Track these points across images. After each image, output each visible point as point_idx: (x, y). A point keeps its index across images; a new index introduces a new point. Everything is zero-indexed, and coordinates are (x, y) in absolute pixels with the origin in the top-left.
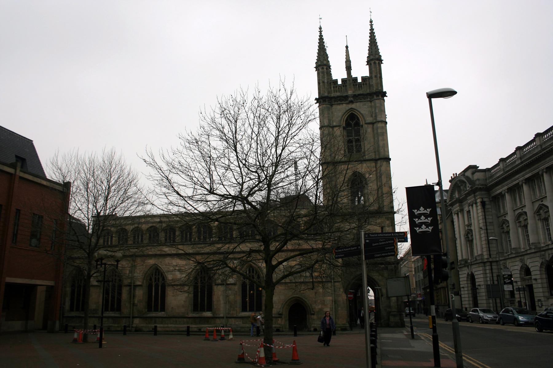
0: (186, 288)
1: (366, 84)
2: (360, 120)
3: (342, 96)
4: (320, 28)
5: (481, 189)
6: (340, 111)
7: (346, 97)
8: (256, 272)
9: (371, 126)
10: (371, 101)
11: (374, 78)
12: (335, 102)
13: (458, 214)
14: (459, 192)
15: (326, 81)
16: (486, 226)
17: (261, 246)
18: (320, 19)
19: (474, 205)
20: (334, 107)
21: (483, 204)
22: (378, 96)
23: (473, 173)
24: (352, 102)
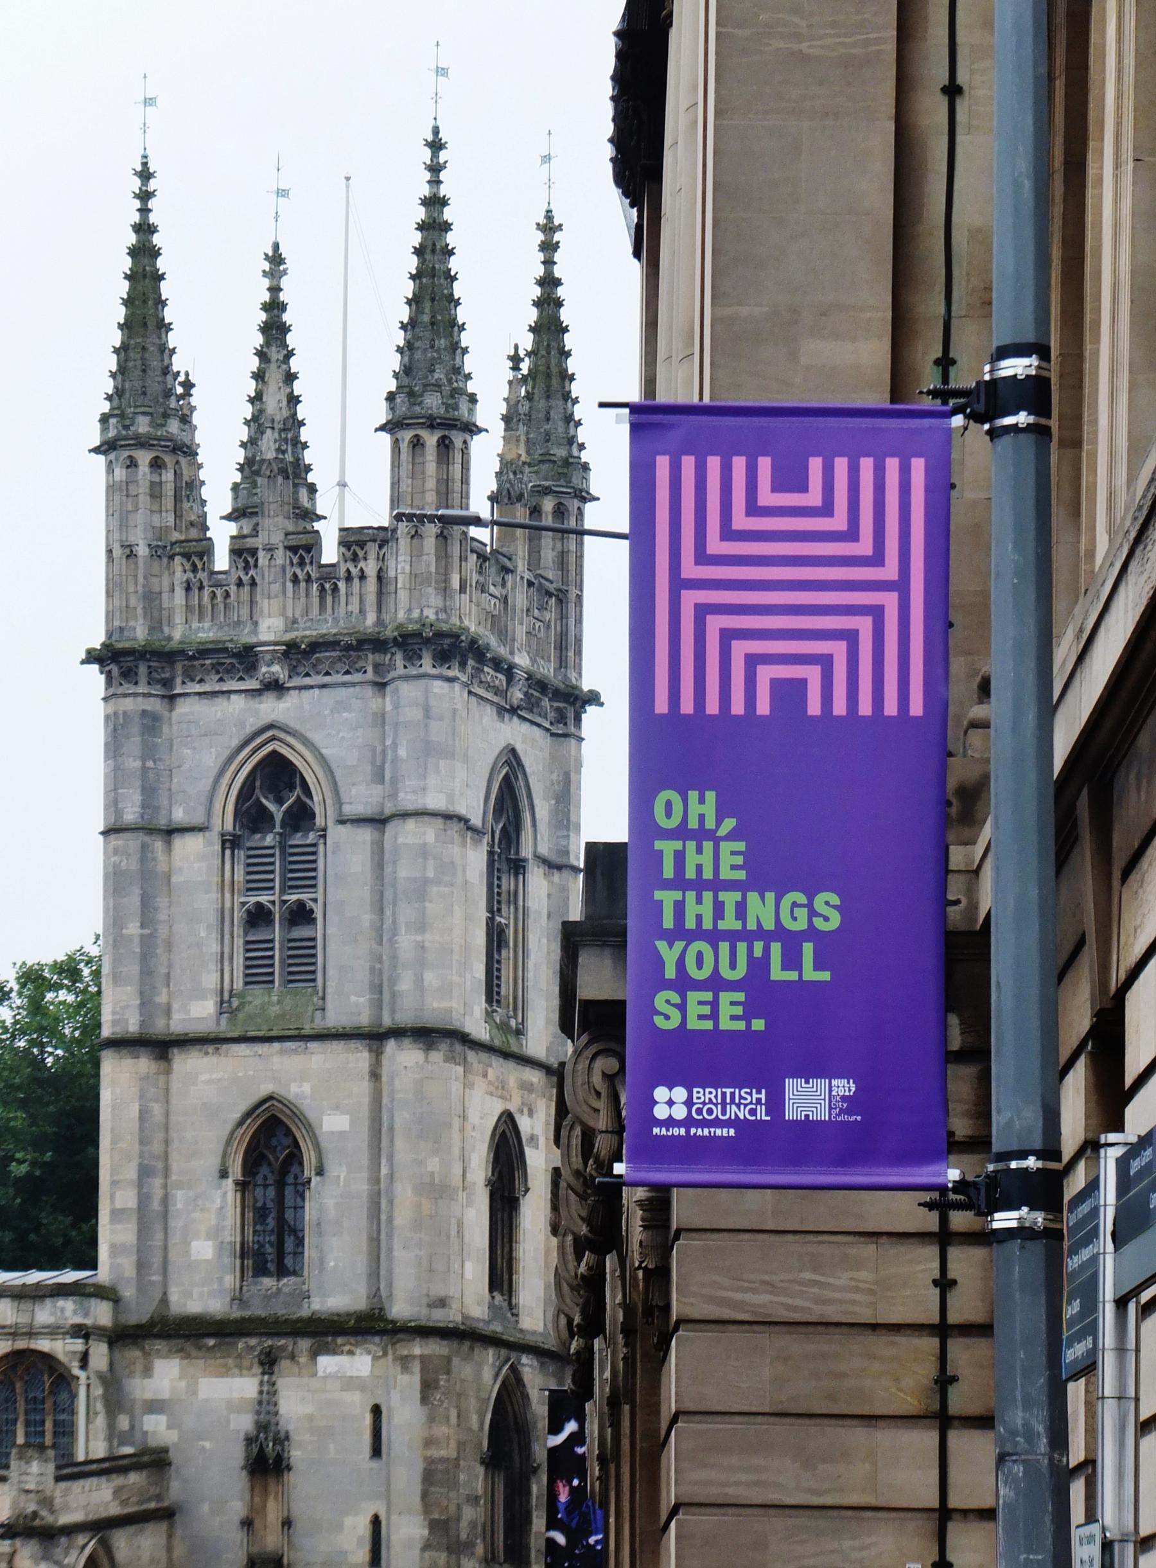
1: (362, 577)
6: (214, 729)
7: (245, 658)
9: (366, 834)
10: (381, 686)
12: (189, 677)
18: (149, 102)
20: (184, 708)
22: (412, 657)
24: (275, 687)
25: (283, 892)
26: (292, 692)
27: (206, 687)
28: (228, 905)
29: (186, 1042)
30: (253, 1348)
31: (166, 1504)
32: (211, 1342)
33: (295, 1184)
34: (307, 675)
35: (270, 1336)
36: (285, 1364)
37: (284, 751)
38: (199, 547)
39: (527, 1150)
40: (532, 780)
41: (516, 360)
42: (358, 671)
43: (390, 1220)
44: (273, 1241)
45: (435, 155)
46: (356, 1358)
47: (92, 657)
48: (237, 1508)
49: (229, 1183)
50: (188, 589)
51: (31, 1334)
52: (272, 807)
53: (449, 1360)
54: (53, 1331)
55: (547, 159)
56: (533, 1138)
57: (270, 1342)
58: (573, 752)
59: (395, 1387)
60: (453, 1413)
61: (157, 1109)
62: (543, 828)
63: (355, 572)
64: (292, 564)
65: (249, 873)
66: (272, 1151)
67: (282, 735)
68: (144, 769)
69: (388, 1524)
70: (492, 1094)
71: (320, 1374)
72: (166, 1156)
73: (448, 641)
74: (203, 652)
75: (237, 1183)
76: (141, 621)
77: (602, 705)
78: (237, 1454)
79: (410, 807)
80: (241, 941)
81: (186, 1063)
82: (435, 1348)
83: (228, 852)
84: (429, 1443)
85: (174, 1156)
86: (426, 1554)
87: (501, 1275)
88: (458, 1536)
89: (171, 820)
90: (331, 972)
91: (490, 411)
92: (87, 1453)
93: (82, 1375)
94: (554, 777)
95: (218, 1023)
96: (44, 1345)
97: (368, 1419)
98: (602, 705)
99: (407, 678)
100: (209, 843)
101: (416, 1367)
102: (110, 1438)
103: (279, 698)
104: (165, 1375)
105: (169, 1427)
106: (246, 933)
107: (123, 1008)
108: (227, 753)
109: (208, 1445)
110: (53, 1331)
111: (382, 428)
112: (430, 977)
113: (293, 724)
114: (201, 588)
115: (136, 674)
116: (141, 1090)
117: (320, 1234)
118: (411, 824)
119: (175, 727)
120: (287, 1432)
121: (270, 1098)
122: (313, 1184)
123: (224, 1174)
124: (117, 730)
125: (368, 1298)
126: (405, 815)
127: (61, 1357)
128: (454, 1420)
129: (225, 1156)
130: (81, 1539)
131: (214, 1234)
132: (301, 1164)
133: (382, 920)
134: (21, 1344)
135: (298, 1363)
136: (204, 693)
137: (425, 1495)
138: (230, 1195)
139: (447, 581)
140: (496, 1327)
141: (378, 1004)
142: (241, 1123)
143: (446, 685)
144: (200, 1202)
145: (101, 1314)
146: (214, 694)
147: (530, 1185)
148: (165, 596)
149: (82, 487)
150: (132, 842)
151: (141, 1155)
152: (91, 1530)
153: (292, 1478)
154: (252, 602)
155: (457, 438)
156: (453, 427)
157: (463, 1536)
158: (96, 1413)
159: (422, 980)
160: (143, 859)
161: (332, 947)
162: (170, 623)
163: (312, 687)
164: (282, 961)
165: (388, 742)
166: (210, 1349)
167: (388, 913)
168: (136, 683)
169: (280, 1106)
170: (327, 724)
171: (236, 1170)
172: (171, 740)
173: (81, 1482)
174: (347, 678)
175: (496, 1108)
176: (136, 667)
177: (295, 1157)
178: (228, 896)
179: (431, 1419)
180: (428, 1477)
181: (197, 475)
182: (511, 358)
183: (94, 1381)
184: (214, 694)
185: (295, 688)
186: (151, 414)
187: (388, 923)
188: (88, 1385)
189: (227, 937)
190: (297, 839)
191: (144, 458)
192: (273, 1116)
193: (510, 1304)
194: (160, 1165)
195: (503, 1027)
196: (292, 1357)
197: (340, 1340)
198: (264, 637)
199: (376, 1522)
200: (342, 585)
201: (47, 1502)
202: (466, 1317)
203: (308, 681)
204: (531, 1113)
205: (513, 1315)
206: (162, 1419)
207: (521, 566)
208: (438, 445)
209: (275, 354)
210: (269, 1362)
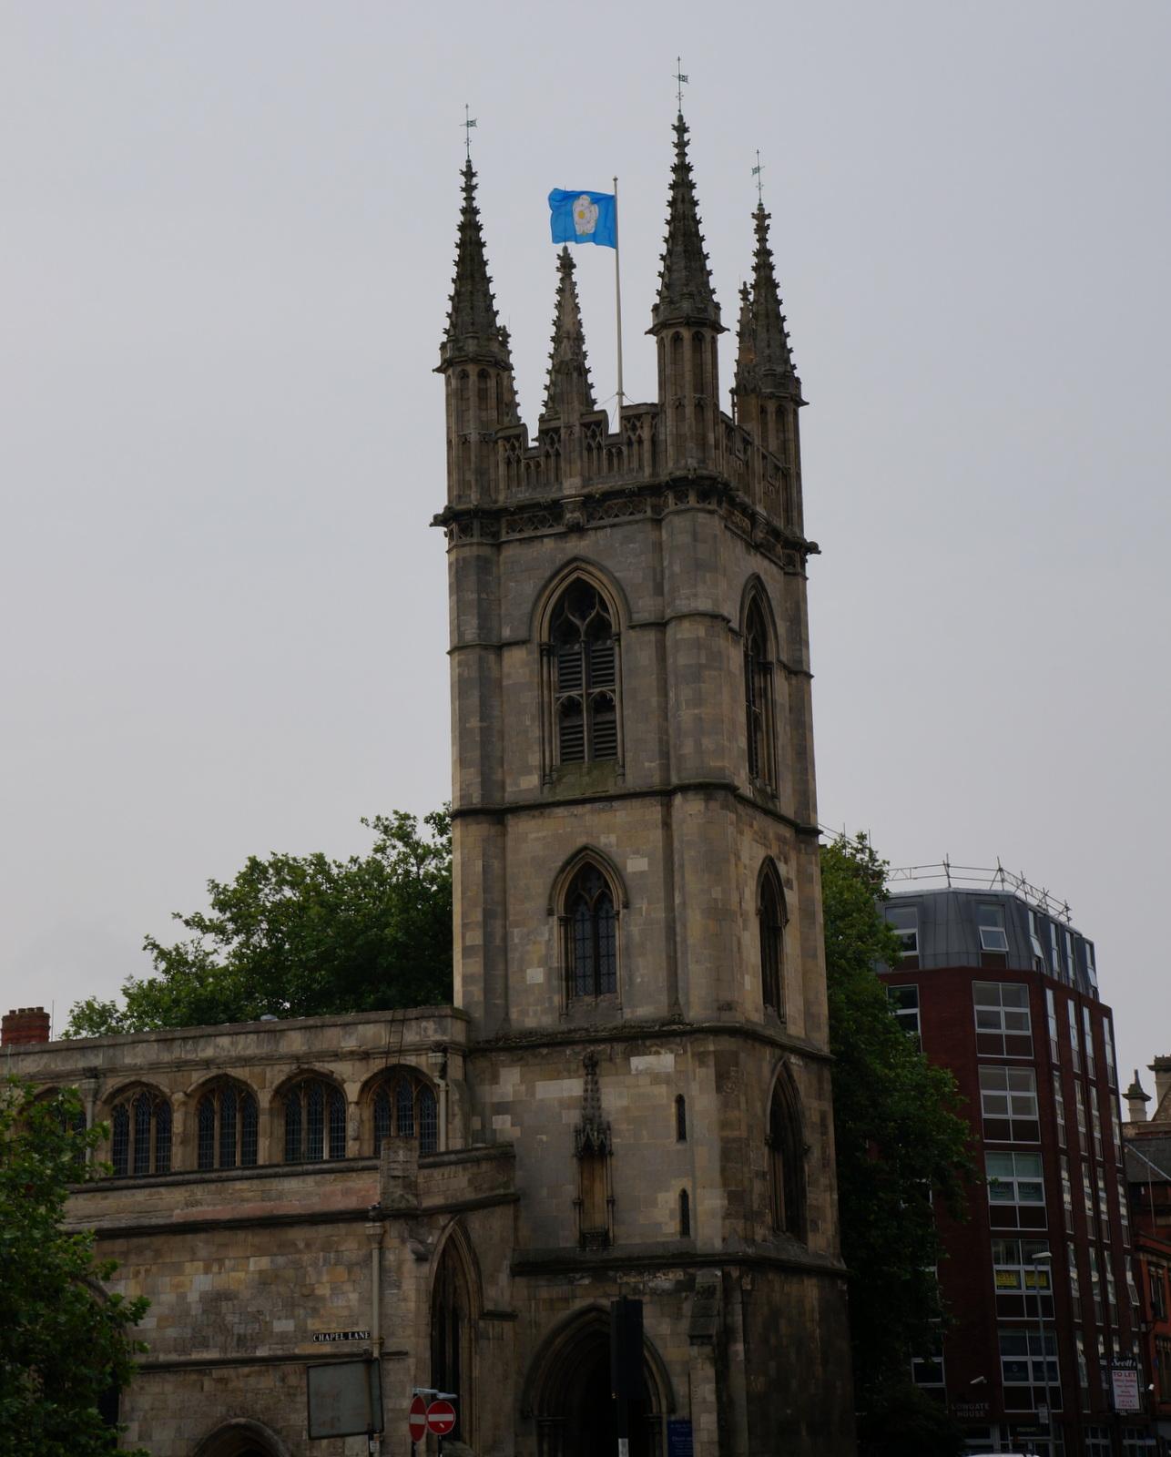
0: (140, 1359)
1: (640, 441)
4: (469, 174)
6: (532, 564)
7: (554, 510)
9: (651, 636)
10: (657, 522)
12: (511, 528)
15: (474, 437)
17: (876, 961)
18: (470, 124)
20: (509, 552)
22: (681, 497)
24: (577, 529)
25: (588, 687)
26: (590, 532)
27: (525, 535)
28: (546, 699)
29: (518, 809)
30: (579, 1053)
31: (512, 1190)
32: (545, 1051)
33: (607, 918)
34: (601, 518)
35: (594, 1046)
36: (604, 1065)
37: (585, 577)
38: (516, 431)
39: (785, 890)
40: (774, 603)
41: (744, 293)
42: (639, 512)
43: (684, 940)
44: (589, 966)
45: (680, 137)
46: (662, 1056)
47: (438, 521)
48: (570, 1191)
49: (554, 920)
50: (509, 463)
51: (401, 1052)
52: (578, 622)
53: (735, 1054)
54: (418, 1049)
55: (757, 170)
56: (789, 881)
57: (592, 1048)
58: (801, 587)
59: (695, 1079)
60: (743, 1099)
62: (782, 643)
63: (634, 438)
64: (586, 437)
65: (562, 675)
66: (587, 892)
67: (583, 565)
68: (480, 600)
69: (694, 1199)
70: (757, 842)
71: (634, 1072)
72: (504, 903)
73: (707, 482)
74: (521, 508)
75: (560, 919)
76: (474, 489)
77: (819, 553)
78: (569, 1145)
79: (685, 610)
80: (558, 728)
82: (727, 1044)
83: (545, 659)
84: (724, 1125)
85: (511, 900)
86: (727, 1222)
87: (772, 992)
88: (752, 1206)
89: (501, 638)
90: (628, 745)
91: (730, 316)
92: (447, 1144)
93: (442, 1083)
94: (788, 605)
95: (542, 792)
96: (411, 1060)
97: (673, 1109)
98: (819, 553)
99: (677, 513)
100: (529, 653)
101: (711, 1062)
102: (465, 1138)
103: (581, 538)
104: (510, 1082)
105: (513, 1125)
106: (561, 721)
107: (467, 786)
108: (543, 582)
109: (544, 1138)
110: (418, 1049)
111: (650, 332)
112: (707, 743)
113: (592, 556)
114: (519, 461)
115: (472, 529)
116: (484, 849)
118: (686, 624)
119: (502, 568)
120: (608, 1123)
121: (585, 848)
122: (621, 916)
123: (550, 913)
124: (459, 574)
125: (669, 1006)
126: (681, 617)
127: (425, 1069)
128: (743, 1106)
129: (551, 898)
130: (442, 1221)
131: (544, 961)
132: (611, 901)
133: (667, 702)
134: (393, 1061)
135: (615, 1064)
136: (524, 539)
137: (723, 1170)
139: (704, 438)
140: (769, 1032)
141: (666, 768)
142: (562, 870)
143: (707, 516)
144: (532, 937)
145: (457, 1032)
146: (531, 539)
147: (789, 916)
148: (492, 471)
149: (430, 396)
150: (472, 656)
151: (485, 902)
152: (450, 1213)
153: (614, 1162)
154: (557, 468)
155: (707, 333)
156: (704, 325)
157: (755, 1207)
158: (454, 1115)
159: (701, 745)
160: (481, 669)
161: (628, 724)
162: (497, 491)
163: (605, 527)
164: (589, 740)
165: (666, 563)
166: (544, 1057)
167: (672, 694)
168: (472, 536)
169: (593, 854)
170: (618, 556)
172: (499, 578)
173: (441, 1170)
174: (631, 518)
175: (761, 853)
176: (472, 523)
177: (605, 897)
178: (546, 692)
179: (725, 1105)
180: (726, 1155)
181: (513, 399)
182: (740, 292)
183: (452, 1088)
184: (531, 539)
185: (591, 529)
186: (478, 338)
187: (672, 701)
188: (447, 1092)
189: (546, 724)
190: (598, 646)
191: (472, 370)
192: (588, 863)
193: (779, 1015)
194: (499, 909)
195: (761, 791)
196: (611, 1060)
197: (648, 1043)
198: (567, 492)
199: (684, 1196)
200: (624, 449)
201: (410, 1185)
202: (748, 1021)
203: (602, 523)
204: (786, 863)
205: (782, 1022)
206: (508, 1118)
207: (757, 441)
208: (694, 339)
209: (568, 308)
210: (591, 1067)
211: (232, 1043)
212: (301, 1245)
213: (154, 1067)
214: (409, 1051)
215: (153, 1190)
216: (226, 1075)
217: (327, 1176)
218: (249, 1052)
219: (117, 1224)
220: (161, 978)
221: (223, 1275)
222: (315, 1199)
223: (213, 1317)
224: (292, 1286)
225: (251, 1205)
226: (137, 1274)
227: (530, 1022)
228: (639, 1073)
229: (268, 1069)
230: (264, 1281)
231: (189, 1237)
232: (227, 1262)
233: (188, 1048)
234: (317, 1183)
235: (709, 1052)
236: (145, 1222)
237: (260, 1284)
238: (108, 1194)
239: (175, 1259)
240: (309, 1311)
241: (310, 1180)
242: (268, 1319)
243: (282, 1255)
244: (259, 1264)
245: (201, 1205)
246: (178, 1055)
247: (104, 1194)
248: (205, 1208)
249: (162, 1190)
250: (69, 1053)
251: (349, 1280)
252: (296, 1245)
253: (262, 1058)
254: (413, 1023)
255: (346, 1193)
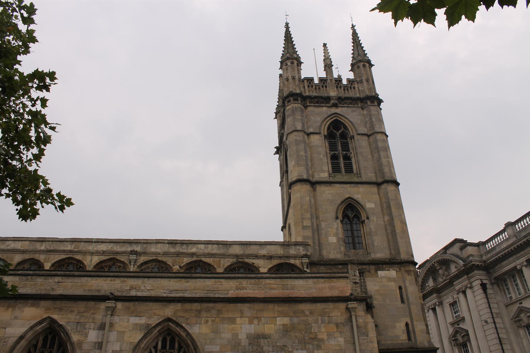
1: (354, 88)
2: (350, 129)
3: (321, 97)
5: (478, 267)
7: (327, 99)
8: (180, 347)
11: (365, 82)
12: (310, 102)
13: (434, 310)
14: (435, 280)
16: (493, 318)
19: (468, 292)
20: (310, 109)
21: (484, 286)
23: (462, 249)
24: (335, 106)
32: (340, 267)
36: (367, 274)
50: (308, 87)
54: (295, 257)
61: (313, 200)
75: (341, 221)
81: (320, 189)
97: (398, 291)
103: (336, 108)
110: (295, 257)
117: (371, 236)
123: (337, 218)
129: (337, 213)
131: (336, 235)
134: (282, 261)
138: (340, 224)
171: (340, 216)
196: (369, 271)
197: (384, 266)
199: (407, 325)
211: (205, 248)
212: (307, 313)
213: (165, 254)
214: (291, 257)
215: (217, 280)
216: (201, 261)
217: (320, 280)
218: (214, 252)
219: (194, 295)
220: (463, 17)
221: (261, 325)
222: (314, 290)
223: (255, 348)
224: (304, 333)
225: (277, 291)
226: (207, 322)
227: (332, 256)
228: (382, 277)
229: (222, 260)
230: (286, 330)
231: (239, 305)
232: (263, 319)
233: (183, 247)
234: (314, 283)
235: (411, 271)
236: (212, 295)
237: (284, 331)
238: (189, 280)
239: (231, 315)
240: (316, 347)
241: (310, 281)
242: (290, 350)
243: (296, 317)
244: (281, 321)
245: (246, 289)
246: (178, 250)
247: (186, 280)
248: (248, 291)
249: (222, 280)
250: (124, 244)
251: (337, 331)
252: (304, 312)
253: (220, 255)
254: (293, 246)
255: (331, 288)
